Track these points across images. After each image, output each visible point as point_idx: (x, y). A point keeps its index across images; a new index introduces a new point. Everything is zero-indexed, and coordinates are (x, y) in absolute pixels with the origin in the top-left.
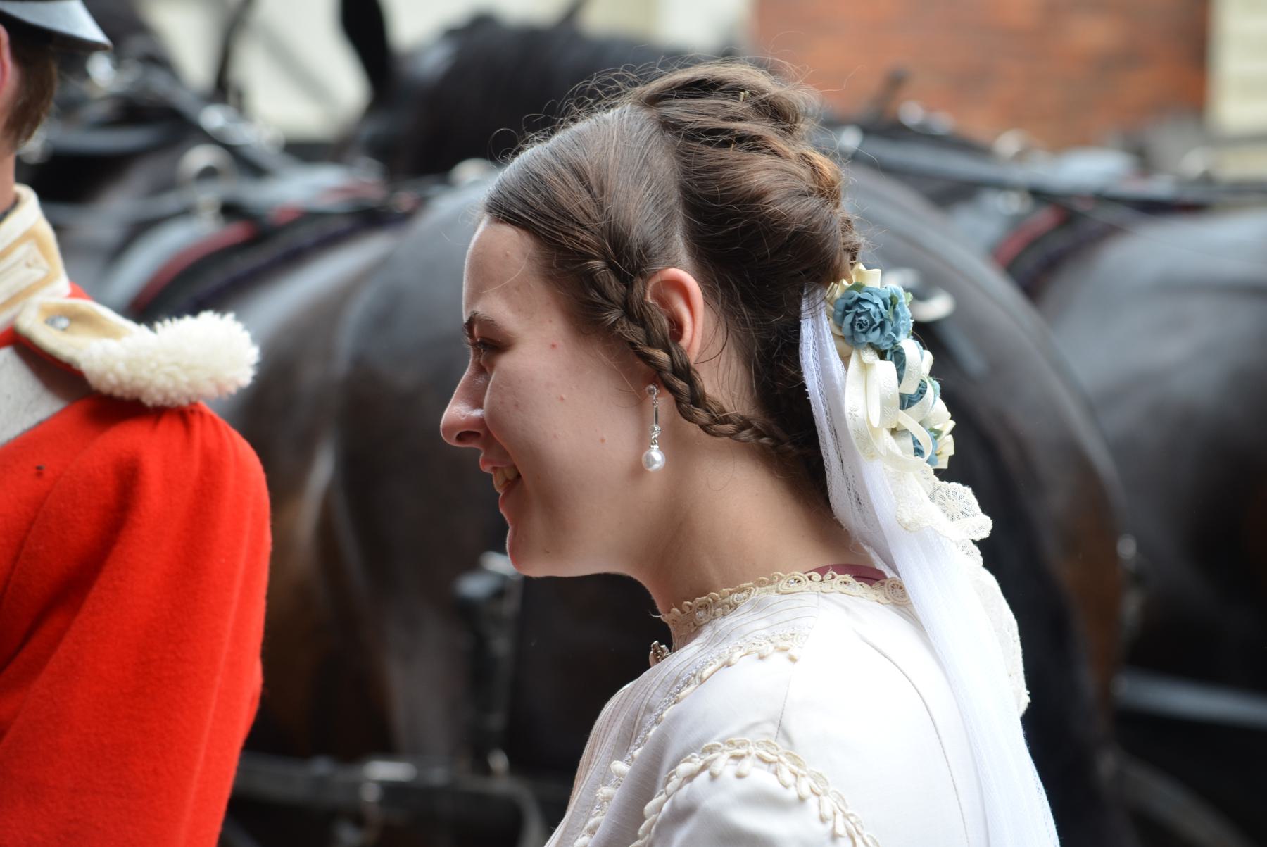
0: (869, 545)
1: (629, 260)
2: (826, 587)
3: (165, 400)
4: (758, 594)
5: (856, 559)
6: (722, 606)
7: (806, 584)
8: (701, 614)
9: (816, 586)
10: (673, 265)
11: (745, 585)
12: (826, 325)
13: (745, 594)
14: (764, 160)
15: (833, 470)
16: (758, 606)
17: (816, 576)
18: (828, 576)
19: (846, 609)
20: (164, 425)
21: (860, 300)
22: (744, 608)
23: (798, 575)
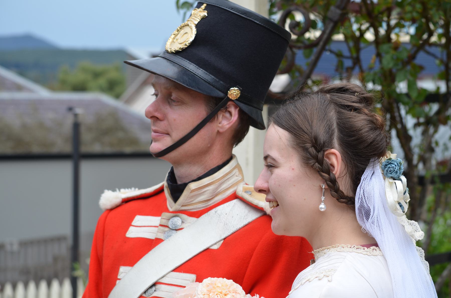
21: (391, 163)
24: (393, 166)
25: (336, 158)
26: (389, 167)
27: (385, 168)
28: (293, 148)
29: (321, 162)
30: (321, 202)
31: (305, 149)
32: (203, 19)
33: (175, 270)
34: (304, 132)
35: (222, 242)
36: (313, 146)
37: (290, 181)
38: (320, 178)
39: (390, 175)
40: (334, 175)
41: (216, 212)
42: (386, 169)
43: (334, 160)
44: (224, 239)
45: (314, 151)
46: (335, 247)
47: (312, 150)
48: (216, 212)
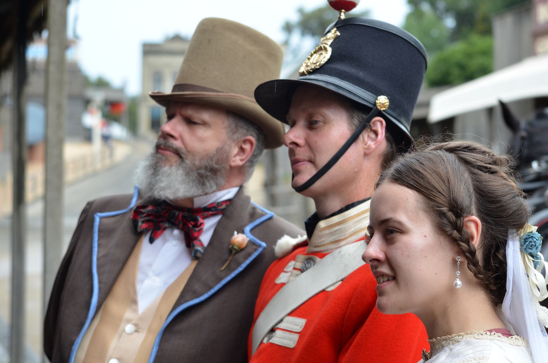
0: (510, 323)
1: (458, 210)
2: (492, 337)
3: (148, 160)
4: (467, 338)
5: (510, 329)
6: (452, 340)
7: (485, 336)
8: (444, 342)
9: (489, 337)
10: (472, 215)
11: (461, 334)
12: (518, 244)
13: (461, 337)
14: (350, 223)
15: (507, 299)
16: (468, 343)
17: (488, 333)
18: (493, 333)
19: (500, 347)
20: (285, 320)
21: (532, 237)
22: (462, 343)
23: (482, 332)
24: (535, 240)
25: (474, 226)
26: (531, 242)
27: (525, 242)
28: (425, 211)
29: (459, 229)
30: (456, 277)
31: (441, 214)
32: (336, 38)
33: (291, 314)
34: (440, 193)
35: (340, 283)
36: (450, 210)
37: (422, 251)
38: (200, 126)
39: (530, 251)
40: (473, 245)
41: (339, 252)
42: (527, 243)
43: (472, 228)
44: (342, 280)
45: (454, 218)
46: (471, 334)
47: (450, 215)
48: (339, 252)
